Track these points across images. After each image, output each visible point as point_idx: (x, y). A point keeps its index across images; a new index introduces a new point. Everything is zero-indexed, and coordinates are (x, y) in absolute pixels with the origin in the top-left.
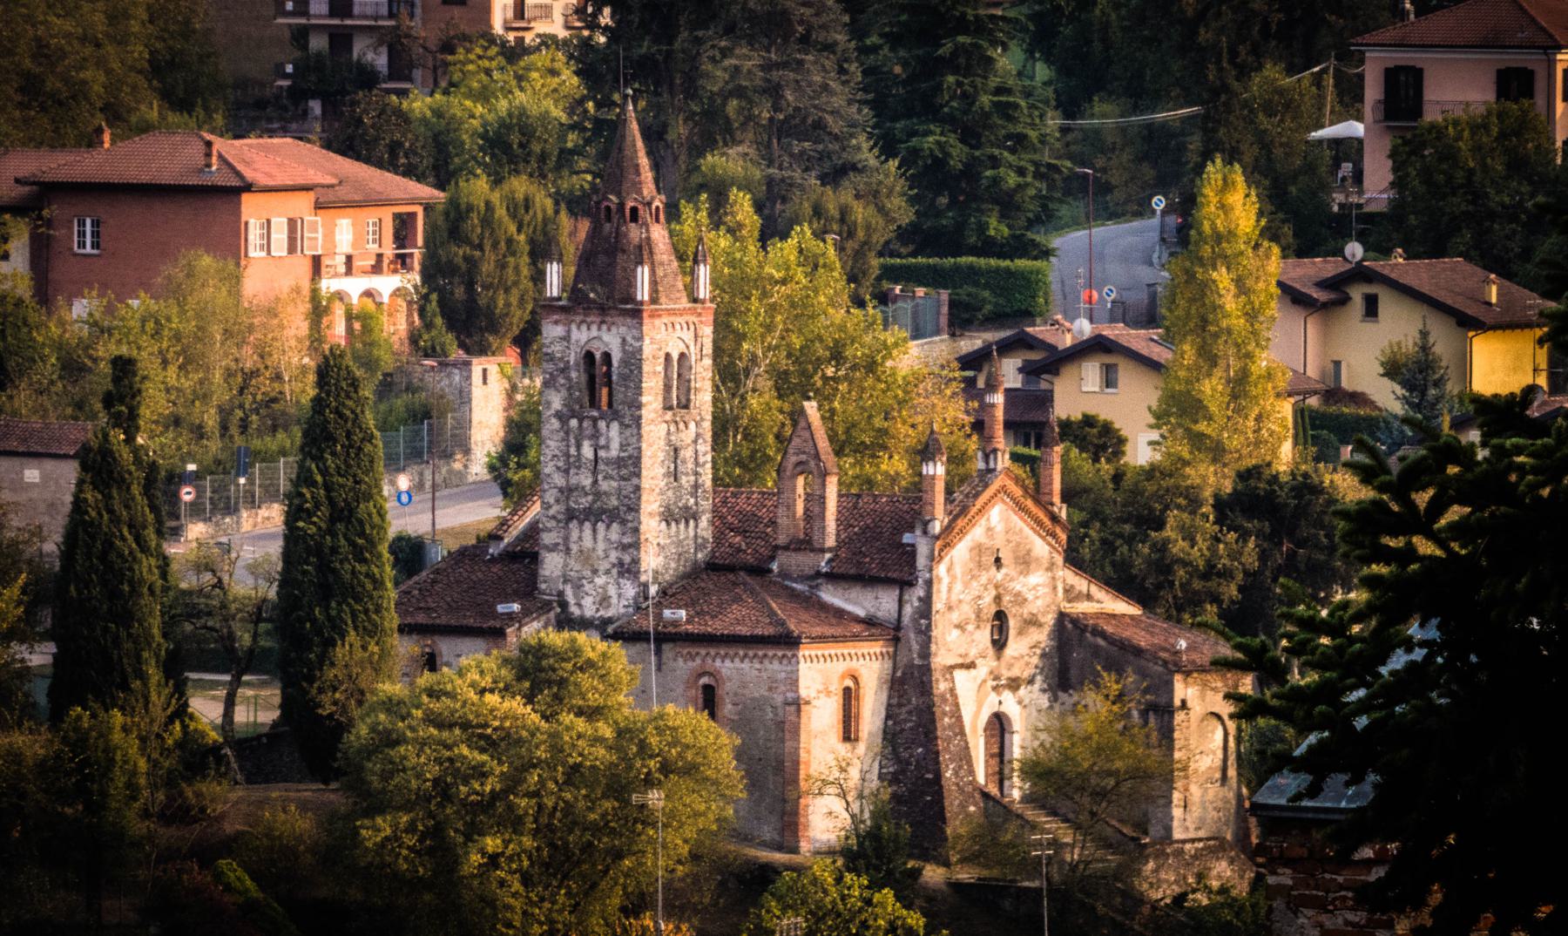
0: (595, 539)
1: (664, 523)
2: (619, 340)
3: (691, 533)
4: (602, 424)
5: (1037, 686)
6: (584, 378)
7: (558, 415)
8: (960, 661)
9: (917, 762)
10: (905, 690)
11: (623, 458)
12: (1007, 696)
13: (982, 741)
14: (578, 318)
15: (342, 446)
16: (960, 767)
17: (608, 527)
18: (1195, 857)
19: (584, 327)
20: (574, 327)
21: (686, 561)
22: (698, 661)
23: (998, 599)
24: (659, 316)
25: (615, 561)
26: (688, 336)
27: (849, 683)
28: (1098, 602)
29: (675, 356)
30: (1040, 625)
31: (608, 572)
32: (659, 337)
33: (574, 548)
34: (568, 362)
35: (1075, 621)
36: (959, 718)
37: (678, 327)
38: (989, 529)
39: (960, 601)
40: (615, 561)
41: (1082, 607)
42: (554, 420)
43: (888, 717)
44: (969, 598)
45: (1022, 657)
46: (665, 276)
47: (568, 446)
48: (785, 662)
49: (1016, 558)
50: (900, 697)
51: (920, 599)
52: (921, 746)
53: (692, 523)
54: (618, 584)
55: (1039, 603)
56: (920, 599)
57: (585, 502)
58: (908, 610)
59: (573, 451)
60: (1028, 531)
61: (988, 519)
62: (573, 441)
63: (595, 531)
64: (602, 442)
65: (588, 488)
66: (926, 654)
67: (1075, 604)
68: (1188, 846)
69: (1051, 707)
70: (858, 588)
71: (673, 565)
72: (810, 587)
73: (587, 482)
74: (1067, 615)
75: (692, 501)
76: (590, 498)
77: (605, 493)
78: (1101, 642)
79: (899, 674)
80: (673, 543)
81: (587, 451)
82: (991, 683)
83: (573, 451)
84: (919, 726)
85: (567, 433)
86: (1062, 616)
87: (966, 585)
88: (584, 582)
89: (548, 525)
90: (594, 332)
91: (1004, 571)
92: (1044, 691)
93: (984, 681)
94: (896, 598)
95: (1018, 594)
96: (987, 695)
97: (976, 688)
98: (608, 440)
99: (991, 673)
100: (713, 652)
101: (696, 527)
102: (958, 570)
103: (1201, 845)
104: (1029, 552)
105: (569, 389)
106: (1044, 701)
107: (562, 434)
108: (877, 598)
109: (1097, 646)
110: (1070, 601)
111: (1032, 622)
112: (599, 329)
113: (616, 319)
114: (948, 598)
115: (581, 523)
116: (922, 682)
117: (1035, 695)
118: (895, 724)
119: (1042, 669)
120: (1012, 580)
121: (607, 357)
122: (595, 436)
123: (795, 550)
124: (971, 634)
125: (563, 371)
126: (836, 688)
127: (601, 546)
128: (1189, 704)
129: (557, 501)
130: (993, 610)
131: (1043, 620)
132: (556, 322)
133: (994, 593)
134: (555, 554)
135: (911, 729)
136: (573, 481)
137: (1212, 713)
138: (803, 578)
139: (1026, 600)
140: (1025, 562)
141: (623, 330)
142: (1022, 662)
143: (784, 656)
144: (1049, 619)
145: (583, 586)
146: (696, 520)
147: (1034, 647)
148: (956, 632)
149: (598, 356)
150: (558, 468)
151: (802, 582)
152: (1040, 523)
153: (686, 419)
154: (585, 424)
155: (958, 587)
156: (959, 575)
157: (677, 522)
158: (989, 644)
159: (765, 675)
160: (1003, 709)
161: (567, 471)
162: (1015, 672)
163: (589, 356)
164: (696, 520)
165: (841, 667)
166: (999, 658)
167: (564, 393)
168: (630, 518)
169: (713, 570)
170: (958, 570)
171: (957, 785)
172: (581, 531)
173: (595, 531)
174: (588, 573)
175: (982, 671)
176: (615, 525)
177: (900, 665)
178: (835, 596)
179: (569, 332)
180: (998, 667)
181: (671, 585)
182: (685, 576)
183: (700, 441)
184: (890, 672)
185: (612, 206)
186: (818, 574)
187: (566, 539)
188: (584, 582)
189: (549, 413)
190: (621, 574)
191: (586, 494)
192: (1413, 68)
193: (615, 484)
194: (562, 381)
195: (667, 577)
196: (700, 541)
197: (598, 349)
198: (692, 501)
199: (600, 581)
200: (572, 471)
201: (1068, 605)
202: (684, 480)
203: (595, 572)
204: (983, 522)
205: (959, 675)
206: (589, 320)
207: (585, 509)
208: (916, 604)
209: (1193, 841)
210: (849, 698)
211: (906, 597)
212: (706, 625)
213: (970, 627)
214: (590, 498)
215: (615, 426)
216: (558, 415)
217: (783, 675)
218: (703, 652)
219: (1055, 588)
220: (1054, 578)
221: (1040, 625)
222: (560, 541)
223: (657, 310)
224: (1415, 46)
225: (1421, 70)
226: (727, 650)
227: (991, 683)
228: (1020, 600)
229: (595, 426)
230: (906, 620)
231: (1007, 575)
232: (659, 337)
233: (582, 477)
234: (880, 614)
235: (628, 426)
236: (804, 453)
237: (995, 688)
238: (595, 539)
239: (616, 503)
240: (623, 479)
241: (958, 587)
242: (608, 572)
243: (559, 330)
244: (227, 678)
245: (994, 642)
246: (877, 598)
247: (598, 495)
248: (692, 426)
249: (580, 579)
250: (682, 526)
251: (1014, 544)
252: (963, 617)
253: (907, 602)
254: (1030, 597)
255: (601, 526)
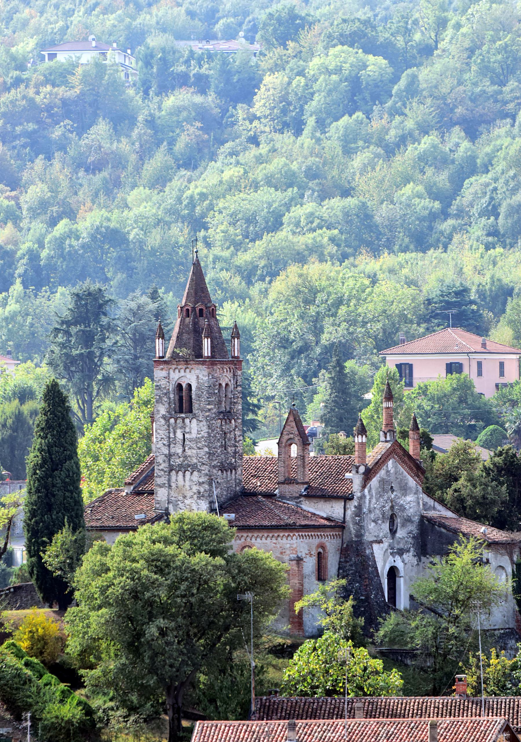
0: (184, 480)
1: (220, 471)
2: (195, 377)
3: (234, 477)
4: (187, 421)
5: (411, 554)
6: (177, 397)
7: (164, 417)
8: (375, 539)
9: (356, 590)
10: (348, 554)
11: (199, 438)
12: (398, 558)
13: (386, 581)
14: (174, 367)
15: (57, 431)
16: (378, 593)
17: (192, 473)
18: (500, 638)
19: (177, 371)
20: (171, 371)
21: (231, 491)
22: (243, 540)
23: (392, 507)
24: (216, 364)
25: (196, 491)
26: (230, 375)
27: (320, 550)
28: (439, 511)
29: (224, 385)
30: (412, 522)
31: (192, 497)
32: (216, 375)
33: (173, 485)
34: (169, 389)
35: (430, 520)
36: (376, 568)
37: (225, 370)
38: (388, 471)
39: (375, 508)
40: (196, 491)
41: (431, 514)
42: (161, 420)
43: (339, 569)
44: (379, 506)
45: (404, 538)
46: (218, 344)
47: (169, 433)
48: (289, 538)
49: (401, 487)
50: (346, 558)
51: (355, 507)
52: (358, 582)
53: (233, 471)
54: (197, 503)
55: (411, 510)
56: (355, 507)
57: (179, 461)
58: (349, 513)
59: (172, 435)
60: (405, 473)
61: (387, 466)
62: (172, 430)
63: (184, 476)
64: (187, 430)
65: (180, 455)
66: (360, 535)
67: (428, 512)
68: (496, 632)
69: (418, 564)
70: (322, 502)
71: (225, 493)
72: (296, 502)
73: (180, 451)
74: (426, 517)
75: (233, 460)
76: (181, 459)
77: (189, 456)
78: (443, 530)
79: (345, 546)
80: (225, 482)
81: (179, 435)
82: (390, 551)
83: (172, 435)
84: (356, 572)
85: (169, 426)
86: (422, 517)
87: (377, 500)
88: (179, 502)
89: (159, 474)
90: (182, 373)
91: (395, 493)
92: (415, 556)
93: (387, 550)
94: (343, 507)
95: (402, 505)
96: (388, 557)
97: (383, 553)
98: (190, 428)
99: (390, 545)
100: (250, 535)
101: (236, 473)
102: (374, 492)
103: (502, 631)
104: (406, 483)
105: (169, 403)
106: (415, 561)
107: (166, 426)
108: (332, 507)
109: (441, 532)
110: (425, 510)
111: (408, 520)
112: (185, 371)
113: (193, 366)
114: (369, 506)
115: (177, 473)
116: (357, 549)
117: (409, 557)
118: (344, 571)
119: (414, 545)
120: (399, 498)
121: (189, 386)
122: (184, 427)
123: (287, 484)
124: (381, 525)
125: (166, 394)
126: (314, 552)
127: (188, 483)
128: (490, 561)
129: (164, 461)
130: (390, 513)
131: (413, 520)
132: (162, 369)
133: (390, 504)
134: (163, 489)
135: (352, 574)
136: (172, 451)
137: (500, 566)
138: (292, 498)
139: (405, 508)
140: (405, 489)
141: (197, 372)
142: (404, 541)
143: (289, 535)
144: (416, 519)
145: (178, 504)
146: (235, 470)
147: (410, 533)
148: (373, 524)
149: (184, 386)
150: (164, 444)
151: (292, 500)
152: (411, 469)
153: (230, 418)
154: (178, 421)
155: (374, 500)
156: (374, 495)
157: (226, 471)
158: (388, 531)
159: (278, 546)
160: (395, 564)
161: (169, 446)
162: (401, 546)
163: (179, 387)
164: (235, 470)
165: (316, 541)
166: (393, 539)
167: (167, 406)
168: (203, 468)
169: (244, 496)
170: (374, 492)
171: (377, 602)
172: (177, 476)
173: (184, 476)
174: (181, 498)
175: (385, 545)
176: (195, 472)
177: (344, 541)
178: (310, 507)
179: (169, 374)
180: (393, 542)
181: (224, 503)
182: (231, 499)
183: (237, 429)
184: (340, 545)
185: (190, 309)
186: (301, 495)
187: (169, 480)
188: (179, 502)
189: (159, 416)
190: (199, 498)
191: (180, 457)
192: (408, 364)
193: (194, 451)
194: (166, 400)
195: (222, 499)
196: (238, 481)
197: (184, 382)
198: (233, 460)
199: (187, 502)
200: (172, 446)
201: (425, 512)
202: (229, 449)
203: (185, 497)
204: (385, 467)
205: (375, 546)
206: (179, 367)
207: (178, 465)
208: (353, 509)
209: (499, 629)
210: (321, 558)
211: (348, 506)
212: (246, 521)
213: (380, 522)
214: (181, 459)
215: (194, 421)
216: (164, 417)
217: (288, 545)
218: (245, 535)
219: (419, 503)
220: (418, 498)
221: (412, 522)
222: (166, 482)
223: (215, 361)
224: (409, 354)
225: (412, 365)
226: (258, 534)
227: (390, 551)
228: (403, 508)
229: (183, 422)
230: (348, 518)
231: (396, 495)
232: (216, 375)
233: (177, 449)
234: (334, 515)
235: (201, 421)
236: (292, 433)
237: (391, 554)
238: (184, 480)
239: (195, 461)
240: (199, 448)
241: (374, 500)
242: (192, 497)
243: (164, 373)
244: (210, 355)
245: (390, 530)
246: (332, 507)
247: (186, 457)
248: (233, 421)
249: (176, 501)
250: (229, 473)
251: (399, 480)
252: (377, 516)
253: (348, 508)
254: (407, 507)
255: (188, 474)
